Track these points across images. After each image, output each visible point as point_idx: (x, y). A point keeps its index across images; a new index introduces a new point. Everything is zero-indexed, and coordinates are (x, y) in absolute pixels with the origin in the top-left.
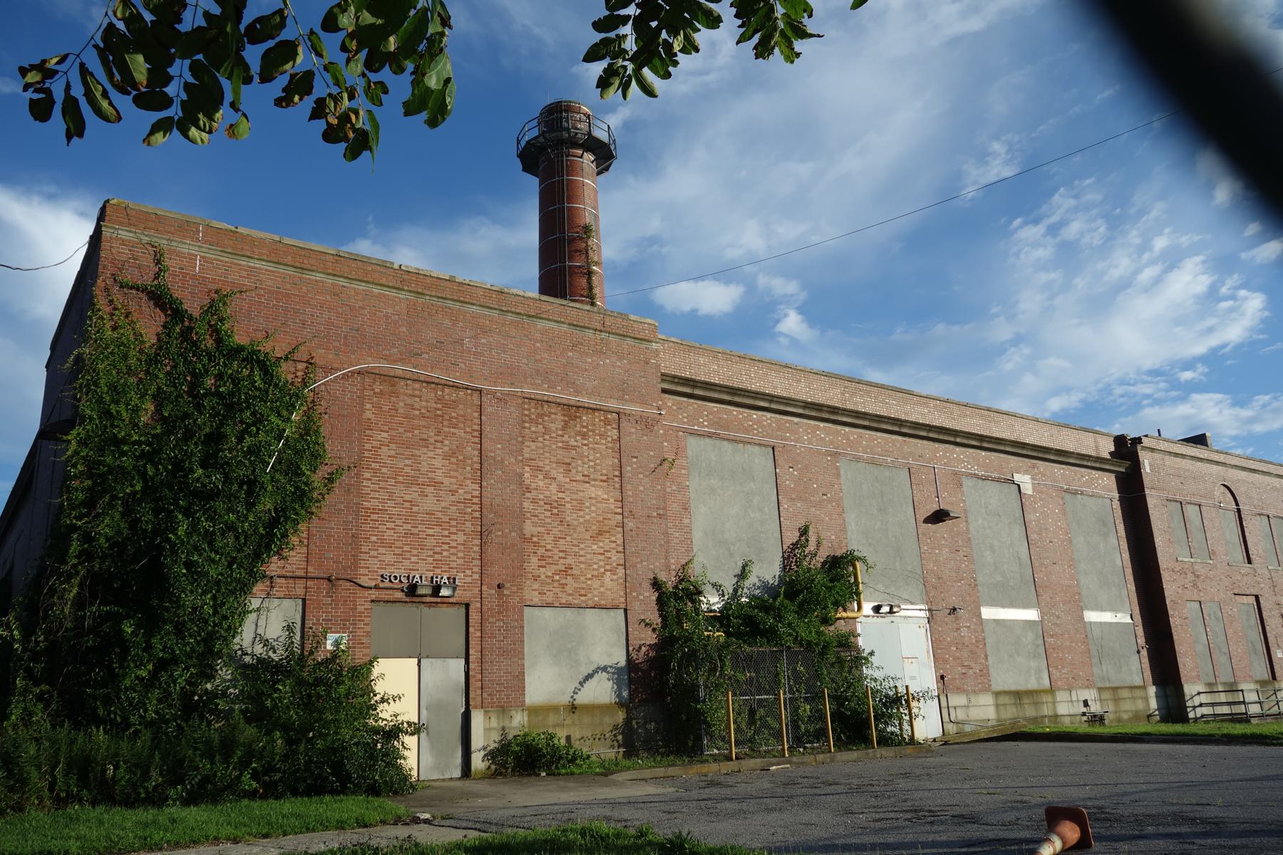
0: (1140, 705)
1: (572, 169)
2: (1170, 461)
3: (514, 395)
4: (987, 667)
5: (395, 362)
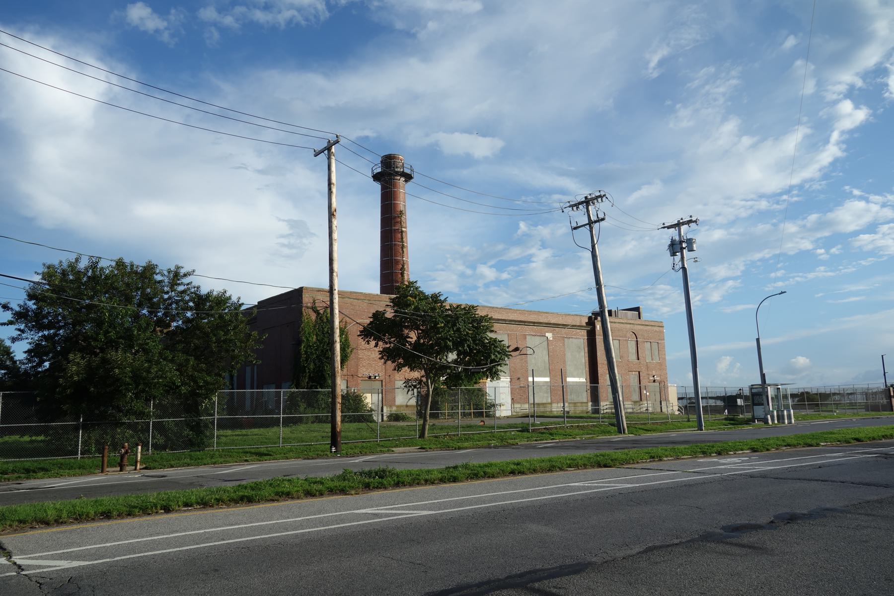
0: (585, 408)
1: (395, 186)
5: (364, 319)
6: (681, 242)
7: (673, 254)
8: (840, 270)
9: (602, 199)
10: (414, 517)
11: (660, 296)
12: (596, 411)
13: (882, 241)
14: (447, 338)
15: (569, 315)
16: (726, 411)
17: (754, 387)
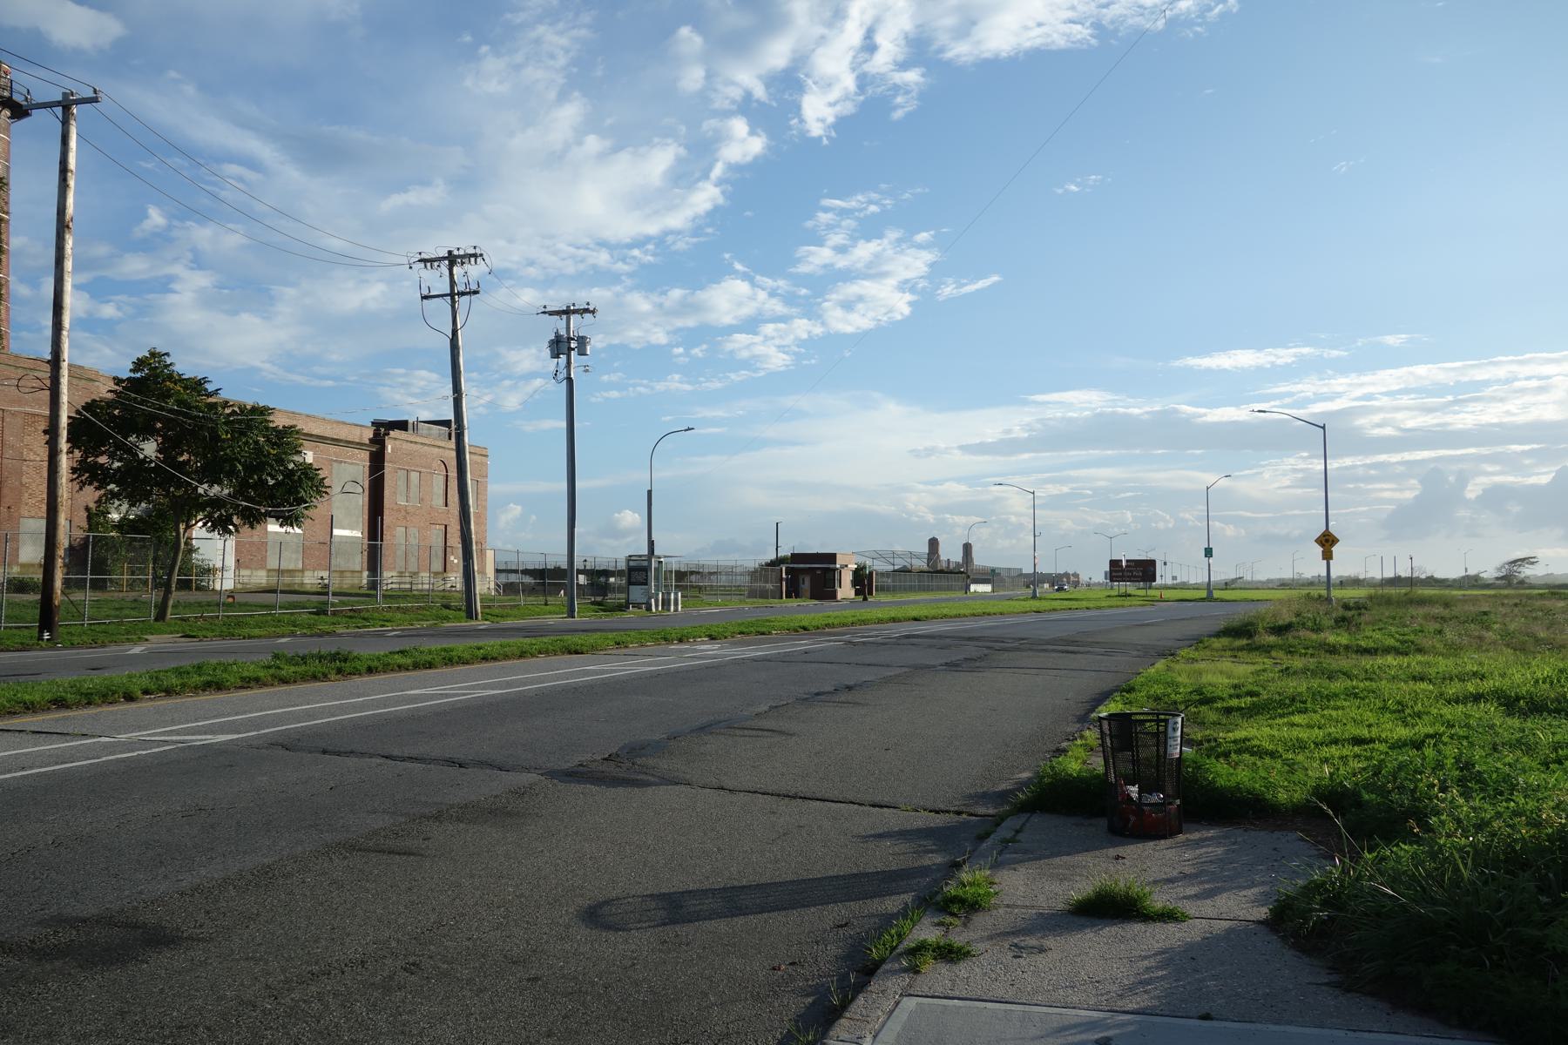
0: (356, 581)
2: (405, 446)
3: (21, 412)
4: (266, 557)
6: (570, 339)
7: (556, 355)
8: (701, 383)
9: (476, 260)
10: (482, 696)
11: (418, 391)
12: (373, 585)
13: (762, 348)
14: (237, 459)
15: (344, 423)
16: (562, 592)
17: (632, 558)
